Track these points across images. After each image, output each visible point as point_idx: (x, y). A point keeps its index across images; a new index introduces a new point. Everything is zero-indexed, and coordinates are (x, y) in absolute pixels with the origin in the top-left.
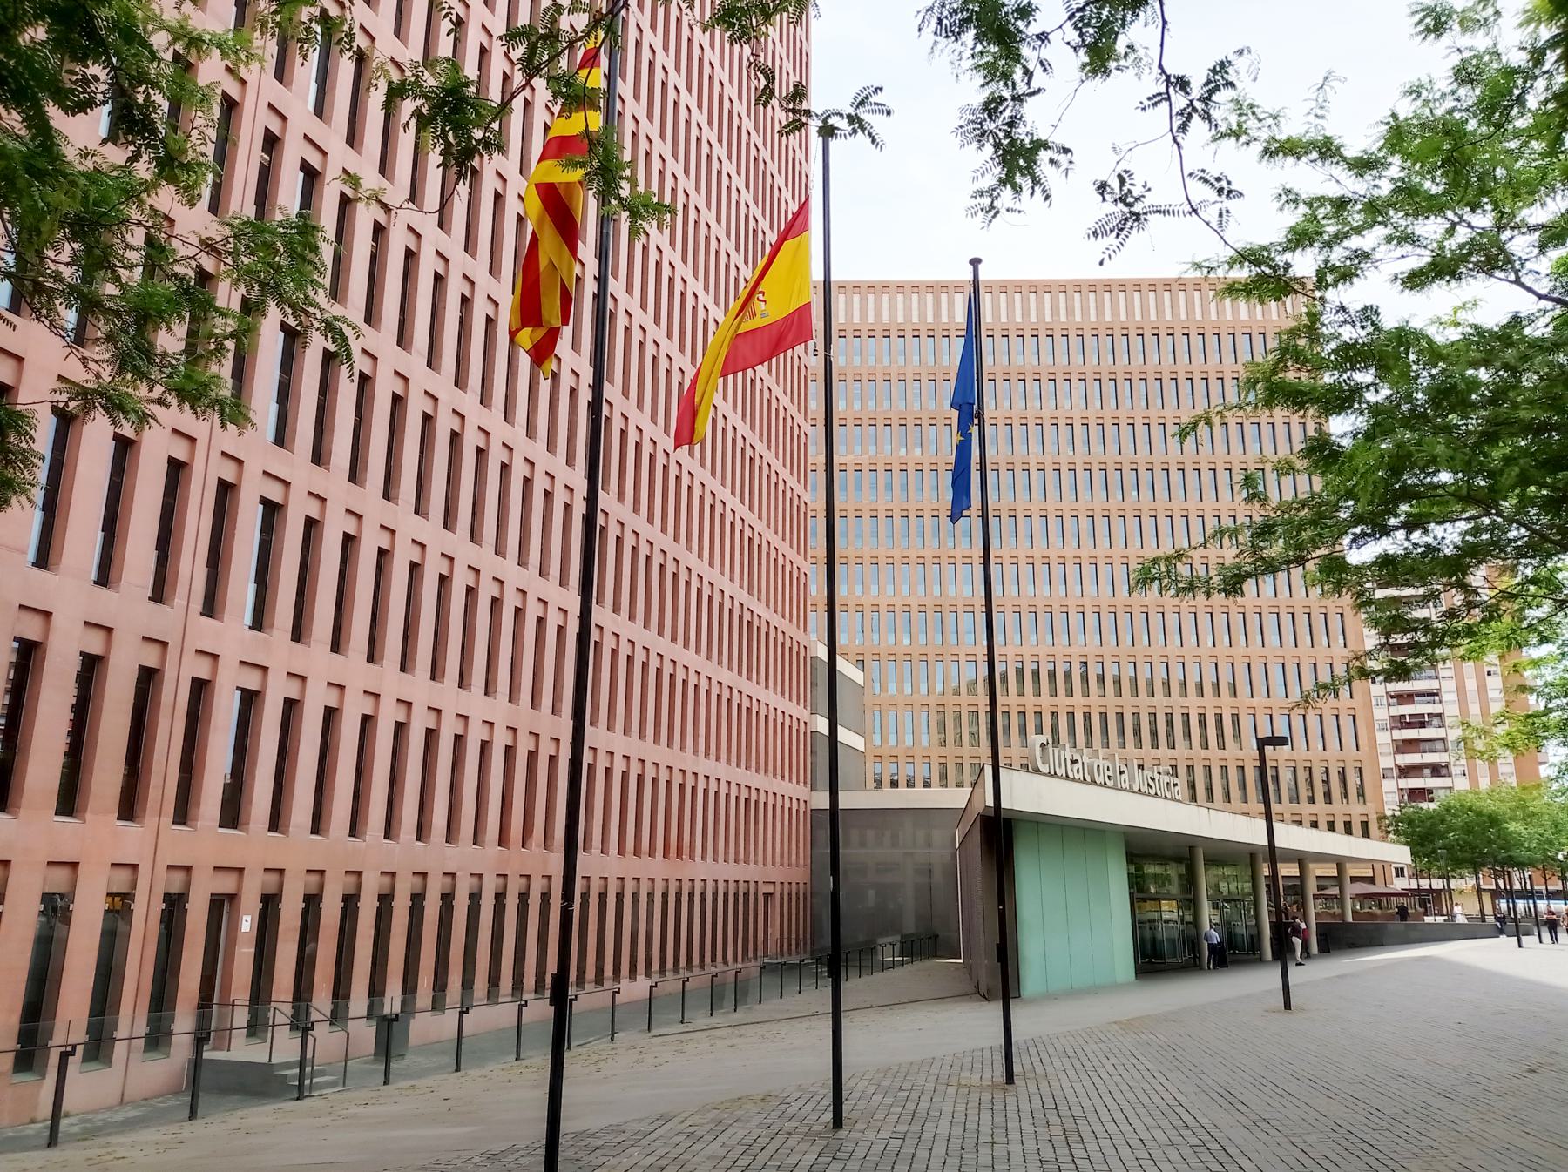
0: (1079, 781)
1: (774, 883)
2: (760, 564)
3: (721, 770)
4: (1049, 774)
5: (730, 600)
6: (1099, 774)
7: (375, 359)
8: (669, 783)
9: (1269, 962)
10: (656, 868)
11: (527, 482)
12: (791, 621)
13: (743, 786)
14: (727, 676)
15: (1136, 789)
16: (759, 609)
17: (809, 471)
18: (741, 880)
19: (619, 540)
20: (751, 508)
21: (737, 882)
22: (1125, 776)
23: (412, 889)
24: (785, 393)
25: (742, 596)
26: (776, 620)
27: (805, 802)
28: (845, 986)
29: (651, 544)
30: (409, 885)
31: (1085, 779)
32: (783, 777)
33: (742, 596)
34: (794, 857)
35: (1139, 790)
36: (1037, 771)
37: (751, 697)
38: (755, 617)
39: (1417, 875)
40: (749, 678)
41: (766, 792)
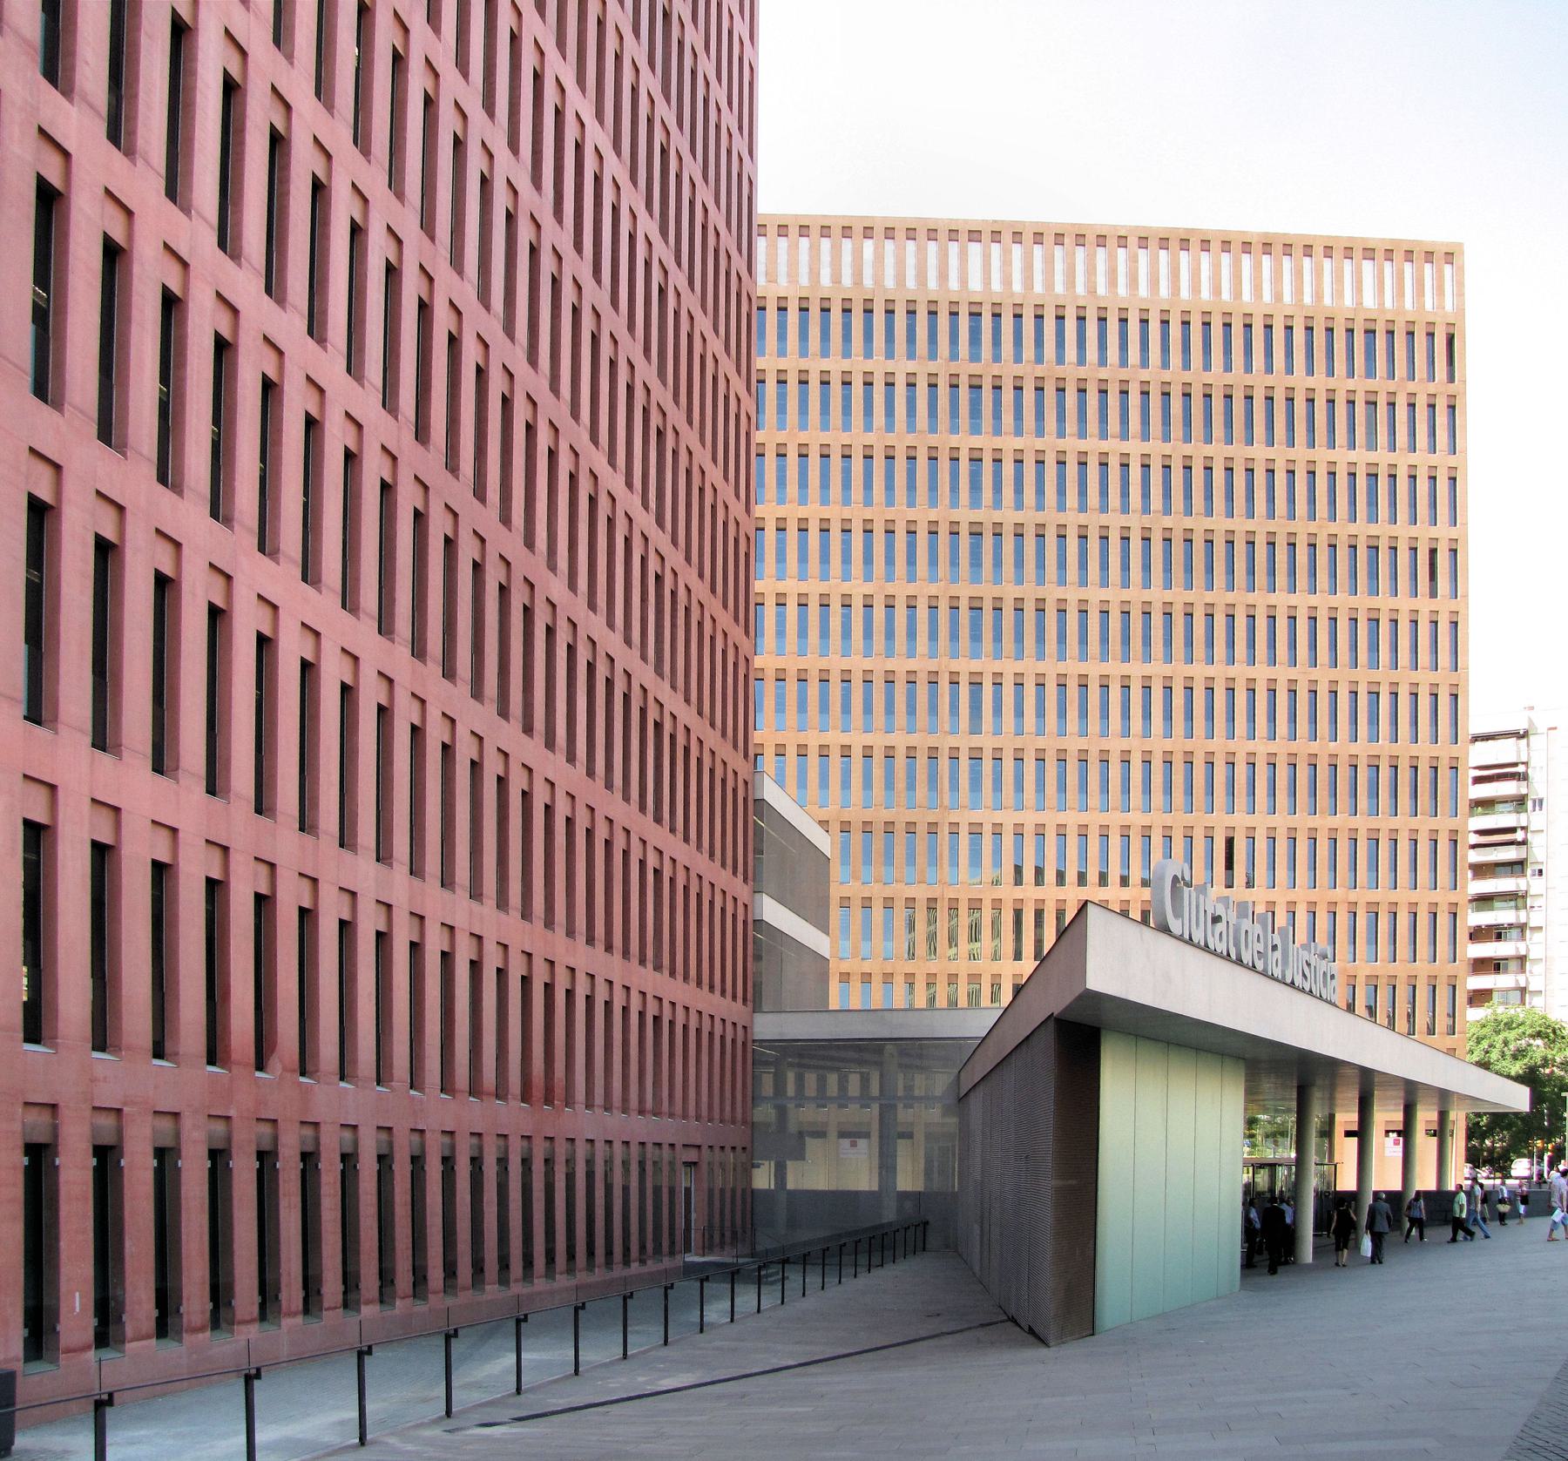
0: (1220, 956)
1: (699, 1147)
2: (674, 626)
3: (612, 966)
4: (1180, 938)
5: (625, 679)
6: (1247, 946)
7: (178, 545)
8: (526, 981)
9: (1308, 1265)
10: (512, 1116)
11: (383, 712)
12: (712, 855)
13: (649, 997)
14: (624, 813)
15: (1289, 981)
16: (674, 702)
17: (753, 455)
18: (649, 1140)
19: (502, 781)
20: (659, 670)
21: (642, 1144)
22: (1278, 954)
23: (24, 1134)
24: (714, 460)
25: (644, 674)
26: (700, 727)
27: (745, 1027)
28: (110, 1438)
29: (530, 770)
30: (17, 1127)
31: (1229, 955)
32: (712, 988)
33: (644, 674)
34: (728, 1108)
35: (1293, 983)
36: (1165, 929)
37: (660, 1000)
38: (667, 862)
39: (1321, 1197)
40: (658, 819)
41: (687, 1009)
